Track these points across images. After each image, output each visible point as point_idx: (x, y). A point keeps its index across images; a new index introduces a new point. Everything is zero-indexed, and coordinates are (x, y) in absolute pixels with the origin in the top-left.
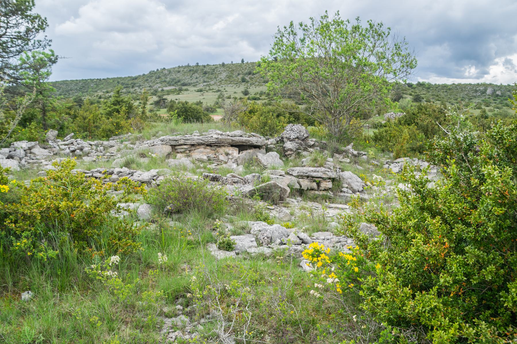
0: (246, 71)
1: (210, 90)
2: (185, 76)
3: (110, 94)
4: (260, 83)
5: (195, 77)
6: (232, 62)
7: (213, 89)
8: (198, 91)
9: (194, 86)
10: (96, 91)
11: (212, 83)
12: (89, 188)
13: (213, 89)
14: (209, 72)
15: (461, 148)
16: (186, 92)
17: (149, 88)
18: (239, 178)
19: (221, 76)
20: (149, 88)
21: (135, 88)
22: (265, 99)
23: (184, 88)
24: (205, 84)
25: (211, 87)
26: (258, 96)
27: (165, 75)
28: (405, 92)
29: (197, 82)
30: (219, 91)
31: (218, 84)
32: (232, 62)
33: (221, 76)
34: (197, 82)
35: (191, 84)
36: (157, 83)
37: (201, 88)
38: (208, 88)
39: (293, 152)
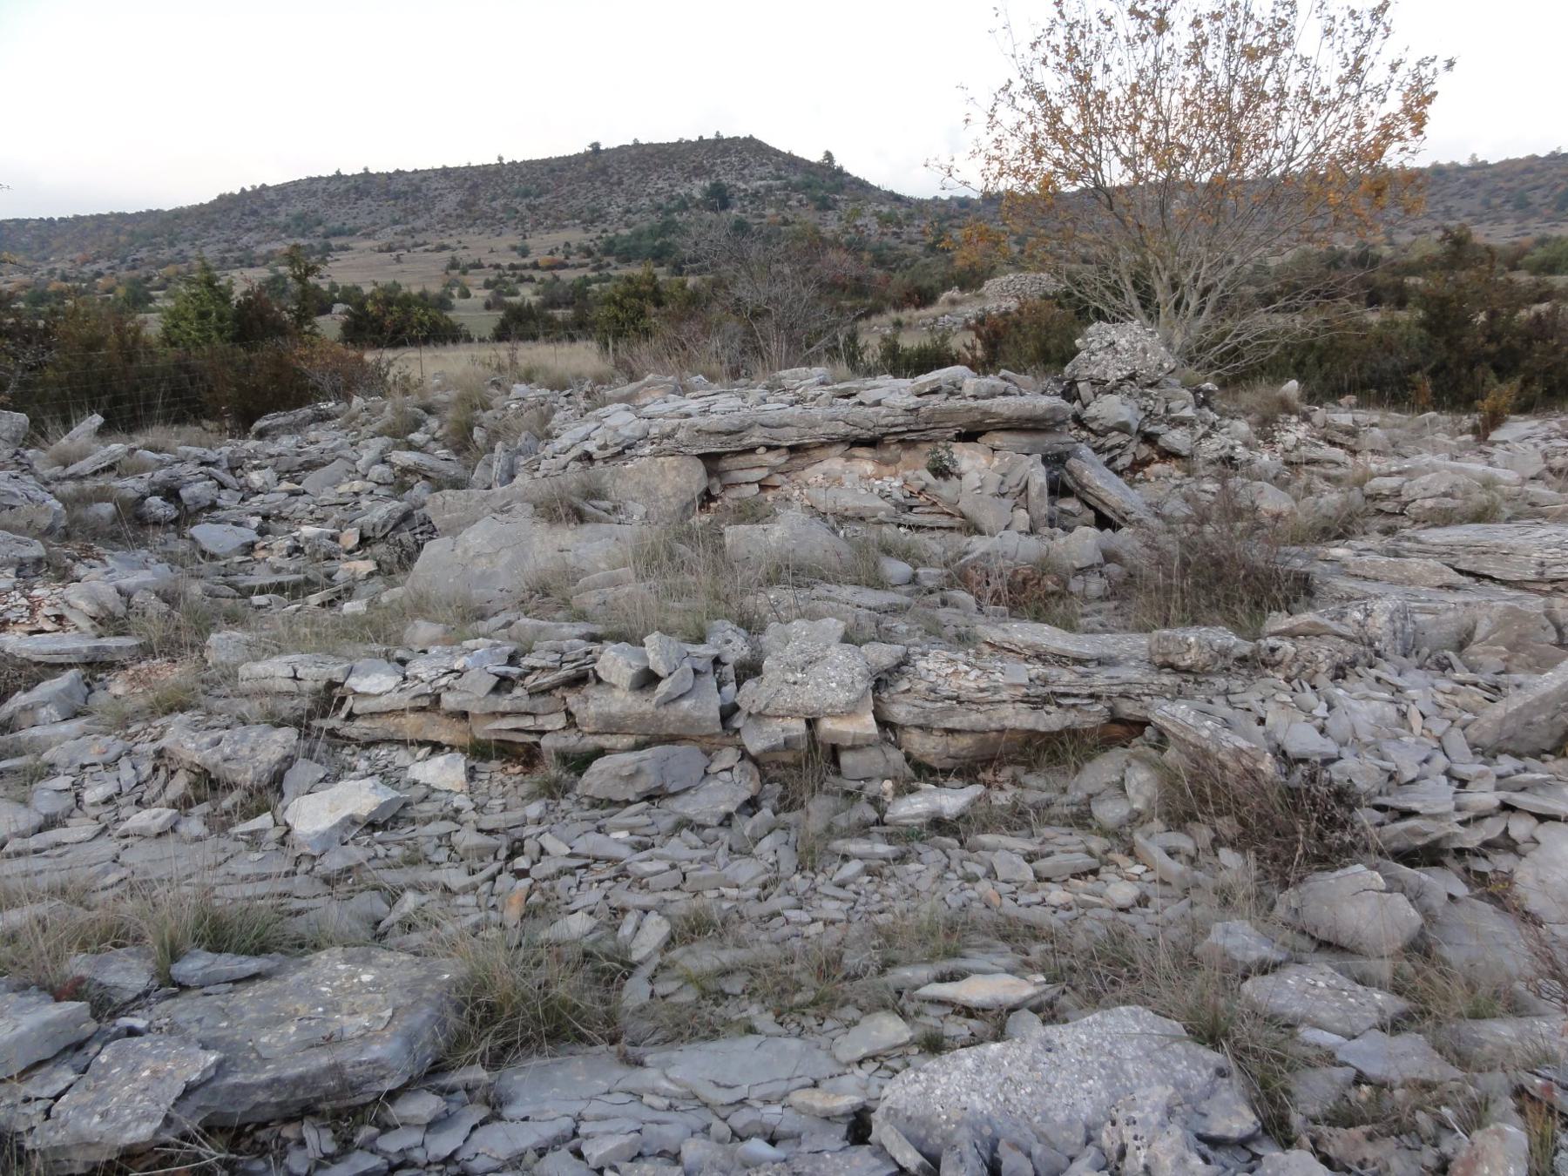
0: (516, 186)
1: (416, 245)
2: (336, 207)
3: (96, 267)
4: (558, 219)
5: (367, 210)
6: (500, 159)
7: (425, 243)
8: (381, 251)
9: (368, 236)
10: (45, 259)
11: (420, 224)
12: (1480, 1071)
13: (425, 243)
14: (405, 193)
15: (177, 628)
16: (343, 256)
17: (226, 245)
18: (1076, 696)
19: (444, 205)
20: (226, 245)
21: (180, 246)
22: (581, 266)
23: (334, 242)
24: (398, 228)
25: (419, 238)
26: (560, 257)
27: (270, 205)
28: (956, 222)
29: (375, 224)
30: (443, 248)
31: (438, 227)
32: (500, 159)
33: (444, 205)
34: (375, 224)
35: (360, 228)
36: (250, 230)
37: (389, 239)
38: (409, 241)
39: (1128, 437)
